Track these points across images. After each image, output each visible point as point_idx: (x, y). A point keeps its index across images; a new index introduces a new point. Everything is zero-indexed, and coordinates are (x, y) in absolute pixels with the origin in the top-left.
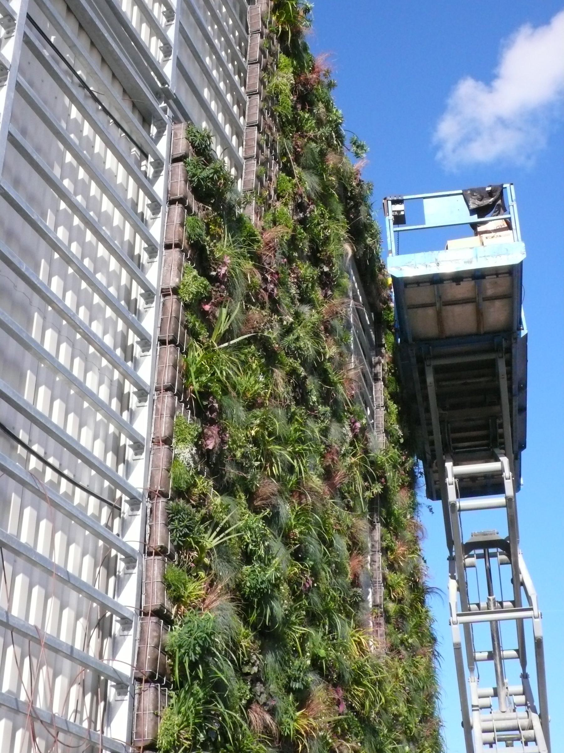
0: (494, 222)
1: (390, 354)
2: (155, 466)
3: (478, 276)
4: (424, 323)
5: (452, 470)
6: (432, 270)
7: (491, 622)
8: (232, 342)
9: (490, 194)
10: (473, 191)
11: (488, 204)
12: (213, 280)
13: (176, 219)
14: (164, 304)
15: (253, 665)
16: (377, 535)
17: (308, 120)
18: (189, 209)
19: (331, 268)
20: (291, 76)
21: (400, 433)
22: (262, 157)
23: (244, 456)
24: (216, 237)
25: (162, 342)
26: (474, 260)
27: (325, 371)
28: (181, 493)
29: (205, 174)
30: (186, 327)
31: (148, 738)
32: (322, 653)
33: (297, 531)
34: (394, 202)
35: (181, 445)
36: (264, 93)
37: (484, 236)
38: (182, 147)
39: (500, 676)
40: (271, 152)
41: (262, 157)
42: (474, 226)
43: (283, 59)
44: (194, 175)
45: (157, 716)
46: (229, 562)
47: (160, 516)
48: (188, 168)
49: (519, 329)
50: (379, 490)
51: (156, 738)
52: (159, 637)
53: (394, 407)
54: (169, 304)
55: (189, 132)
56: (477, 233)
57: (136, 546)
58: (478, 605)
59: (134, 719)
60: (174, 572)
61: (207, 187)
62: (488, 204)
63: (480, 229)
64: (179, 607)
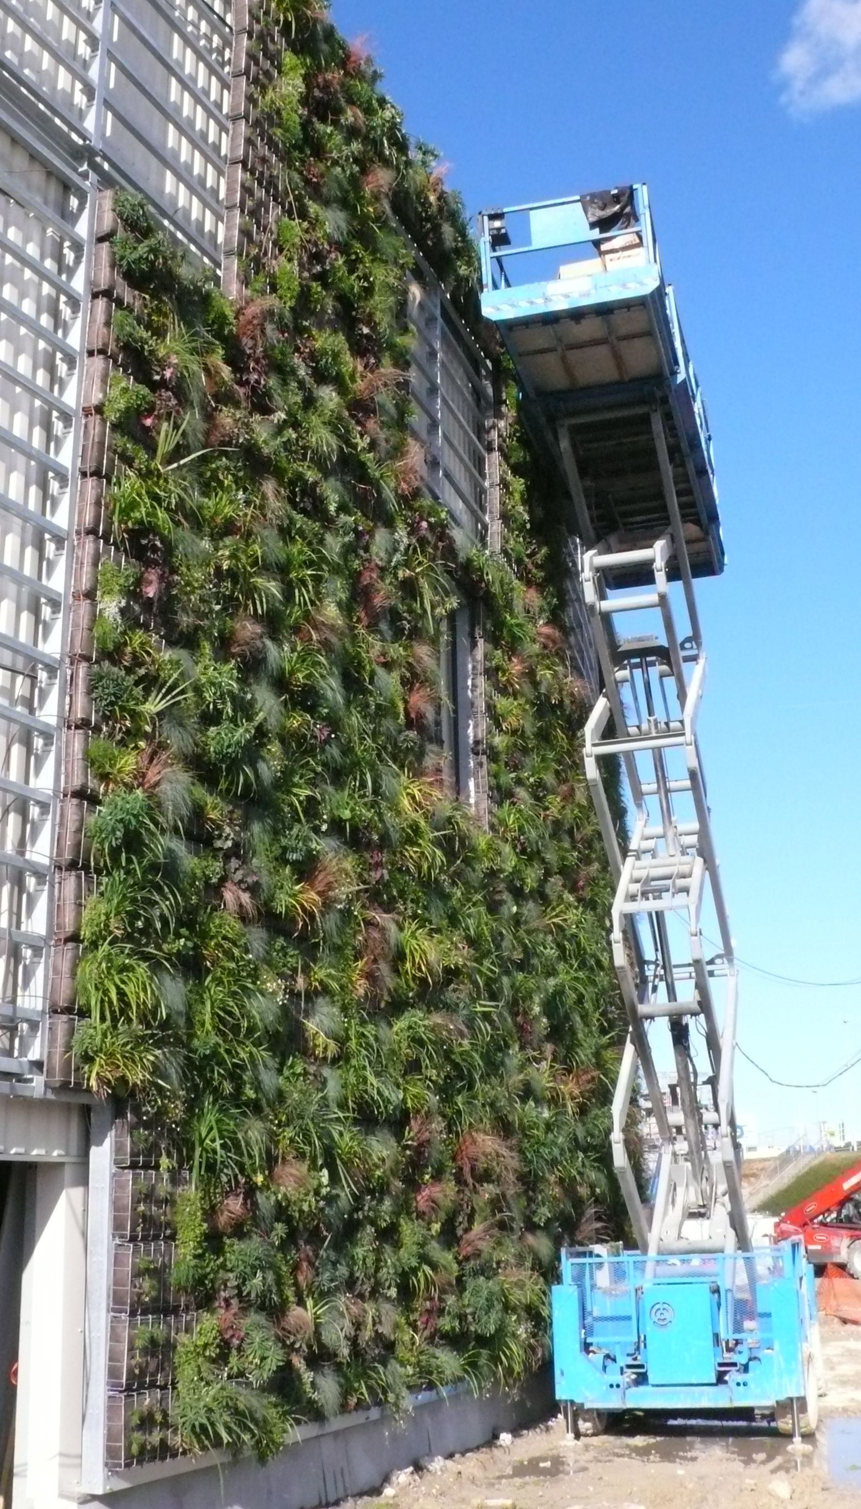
0: (621, 237)
1: (513, 413)
2: (76, 625)
3: (604, 310)
4: (552, 373)
5: (590, 561)
6: (540, 308)
7: (653, 749)
8: (182, 462)
9: (616, 199)
10: (593, 196)
11: (614, 213)
12: (154, 387)
13: (100, 317)
14: (86, 426)
15: (227, 839)
16: (479, 653)
17: (330, 135)
18: (119, 302)
19: (373, 329)
20: (299, 82)
21: (526, 517)
22: (249, 203)
23: (202, 600)
24: (159, 333)
25: (84, 474)
26: (593, 291)
27: (363, 465)
28: (112, 655)
29: (135, 256)
30: (115, 452)
31: (69, 929)
32: (347, 814)
33: (300, 676)
34: (492, 217)
35: (107, 598)
36: (253, 114)
37: (608, 257)
38: (108, 220)
39: (667, 813)
40: (267, 192)
41: (249, 203)
42: (597, 243)
43: (289, 59)
44: (122, 258)
45: (80, 905)
46: (181, 725)
47: (80, 682)
48: (115, 249)
49: (674, 373)
50: (455, 605)
51: (79, 929)
52: (82, 821)
53: (518, 484)
54: (91, 426)
55: (116, 201)
56: (602, 254)
57: (53, 721)
58: (638, 727)
59: (55, 910)
60: (101, 744)
61: (142, 271)
62: (614, 213)
63: (604, 247)
64: (107, 785)
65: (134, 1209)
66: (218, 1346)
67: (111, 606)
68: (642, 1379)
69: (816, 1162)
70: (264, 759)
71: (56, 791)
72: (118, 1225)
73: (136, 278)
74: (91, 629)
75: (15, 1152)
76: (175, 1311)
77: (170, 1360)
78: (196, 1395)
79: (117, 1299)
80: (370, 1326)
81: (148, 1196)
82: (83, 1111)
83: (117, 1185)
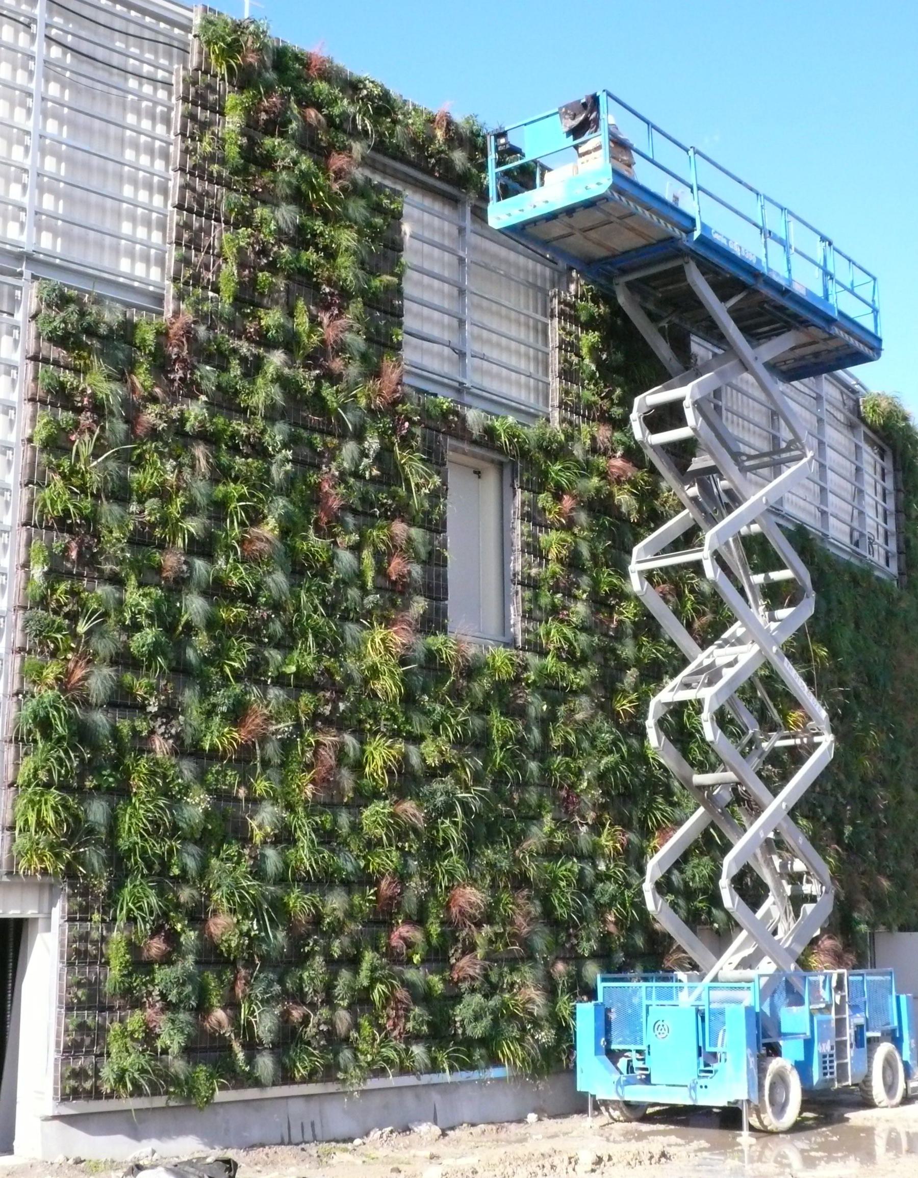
31: (10, 780)
63: (582, 150)
65: (69, 946)
66: (144, 1031)
67: (38, 571)
70: (191, 646)
73: (61, 340)
74: (25, 589)
75: (13, 913)
76: (111, 1009)
77: (104, 1039)
78: (121, 1057)
81: (84, 938)
83: (62, 933)
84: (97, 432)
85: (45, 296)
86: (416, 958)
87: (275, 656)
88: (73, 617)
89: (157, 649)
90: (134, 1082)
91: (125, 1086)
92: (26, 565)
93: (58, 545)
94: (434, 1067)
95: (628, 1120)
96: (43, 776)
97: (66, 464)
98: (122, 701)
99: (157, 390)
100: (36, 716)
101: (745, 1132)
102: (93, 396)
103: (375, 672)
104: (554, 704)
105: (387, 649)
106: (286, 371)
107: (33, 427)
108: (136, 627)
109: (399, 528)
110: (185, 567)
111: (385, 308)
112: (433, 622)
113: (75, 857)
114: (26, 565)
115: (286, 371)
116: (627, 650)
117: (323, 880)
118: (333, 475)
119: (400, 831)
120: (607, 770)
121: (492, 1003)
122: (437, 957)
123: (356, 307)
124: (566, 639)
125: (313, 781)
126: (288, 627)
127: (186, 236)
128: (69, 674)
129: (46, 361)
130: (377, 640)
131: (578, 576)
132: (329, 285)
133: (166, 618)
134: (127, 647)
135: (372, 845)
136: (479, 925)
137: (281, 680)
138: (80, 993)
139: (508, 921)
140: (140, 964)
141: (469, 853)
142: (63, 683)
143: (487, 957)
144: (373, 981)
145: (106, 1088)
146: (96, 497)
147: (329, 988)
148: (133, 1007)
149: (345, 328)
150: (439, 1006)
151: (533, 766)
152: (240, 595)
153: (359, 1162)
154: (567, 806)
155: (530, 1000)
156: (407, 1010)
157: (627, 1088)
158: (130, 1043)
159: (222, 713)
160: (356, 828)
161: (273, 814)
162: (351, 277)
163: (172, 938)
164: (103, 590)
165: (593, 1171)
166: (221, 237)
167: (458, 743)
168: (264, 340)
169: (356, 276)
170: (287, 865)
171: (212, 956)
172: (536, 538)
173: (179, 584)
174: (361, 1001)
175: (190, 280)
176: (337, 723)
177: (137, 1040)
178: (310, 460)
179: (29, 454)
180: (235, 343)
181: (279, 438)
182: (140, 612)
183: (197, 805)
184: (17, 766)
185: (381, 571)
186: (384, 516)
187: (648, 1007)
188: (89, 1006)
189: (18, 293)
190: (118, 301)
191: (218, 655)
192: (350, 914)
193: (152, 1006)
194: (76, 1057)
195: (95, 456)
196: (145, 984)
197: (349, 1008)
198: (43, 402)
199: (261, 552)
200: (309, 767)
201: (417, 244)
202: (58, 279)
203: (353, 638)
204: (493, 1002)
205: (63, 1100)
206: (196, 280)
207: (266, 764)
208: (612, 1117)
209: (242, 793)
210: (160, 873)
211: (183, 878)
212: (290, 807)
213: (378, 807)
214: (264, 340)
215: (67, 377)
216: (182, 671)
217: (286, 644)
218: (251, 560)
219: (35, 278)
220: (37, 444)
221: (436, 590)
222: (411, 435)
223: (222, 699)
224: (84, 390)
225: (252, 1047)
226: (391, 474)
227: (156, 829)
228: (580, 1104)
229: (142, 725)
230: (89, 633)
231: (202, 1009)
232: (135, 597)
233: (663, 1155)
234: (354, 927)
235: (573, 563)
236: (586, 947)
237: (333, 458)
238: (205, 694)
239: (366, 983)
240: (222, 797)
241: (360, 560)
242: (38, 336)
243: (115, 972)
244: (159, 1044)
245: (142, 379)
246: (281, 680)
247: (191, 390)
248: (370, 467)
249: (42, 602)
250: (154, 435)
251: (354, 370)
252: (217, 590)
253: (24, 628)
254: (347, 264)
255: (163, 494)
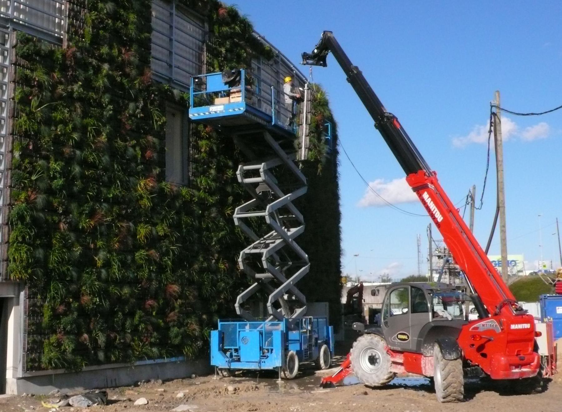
31: (6, 240)
67: (17, 154)
68: (239, 360)
69: (517, 280)
71: (3, 205)
72: (25, 313)
73: (26, 57)
74: (12, 161)
76: (45, 334)
78: (48, 354)
79: (25, 331)
80: (89, 18)
82: (19, 285)
83: (25, 303)
84: (41, 96)
85: (20, 37)
86: (154, 313)
87: (104, 190)
88: (31, 174)
89: (63, 187)
90: (55, 363)
91: (51, 365)
92: (12, 152)
93: (25, 142)
94: (161, 356)
95: (229, 376)
96: (20, 239)
97: (28, 109)
98: (49, 208)
99: (62, 79)
100: (18, 213)
101: (280, 379)
102: (38, 81)
103: (142, 197)
104: (203, 212)
105: (146, 188)
106: (110, 72)
107: (15, 93)
108: (55, 178)
109: (150, 138)
110: (72, 153)
111: (145, 46)
112: (161, 177)
113: (32, 272)
114: (12, 152)
115: (110, 72)
116: (229, 189)
117: (121, 283)
118: (127, 116)
119: (149, 260)
120: (222, 237)
121: (181, 331)
122: (162, 313)
123: (135, 47)
124: (208, 184)
125: (118, 242)
126: (110, 178)
127: (72, 14)
128: (29, 197)
129: (19, 65)
130: (142, 184)
131: (212, 158)
132: (125, 37)
133: (65, 173)
134: (51, 186)
135: (140, 267)
136: (176, 300)
137: (107, 200)
138: (33, 328)
139: (187, 298)
140: (56, 316)
141: (173, 271)
142: (27, 200)
143: (179, 312)
144: (140, 322)
145: (43, 365)
146: (39, 123)
147: (124, 324)
148: (52, 333)
149: (131, 56)
150: (164, 331)
151: (196, 235)
152: (93, 166)
153: (136, 394)
154: (207, 251)
155: (194, 330)
156: (151, 334)
157: (232, 363)
158: (52, 348)
159: (86, 214)
160: (133, 260)
161: (104, 255)
162: (133, 34)
163: (68, 305)
164: (41, 162)
165: (235, 393)
166: (84, 13)
167: (170, 226)
168: (101, 59)
169: (135, 33)
170: (109, 275)
171: (83, 312)
172: (198, 143)
173: (69, 161)
174: (135, 330)
175: (74, 32)
176: (127, 218)
177: (54, 346)
178: (118, 111)
179: (13, 105)
180: (90, 60)
181: (107, 100)
182: (56, 172)
183: (78, 250)
184: (9, 235)
185: (143, 156)
186: (144, 133)
187: (239, 332)
188: (36, 333)
189: (7, 36)
190: (47, 41)
191: (84, 190)
192: (131, 296)
193: (60, 333)
194: (32, 354)
195: (39, 106)
196: (58, 324)
197: (131, 333)
198: (18, 83)
199: (101, 147)
200: (117, 236)
201: (158, 21)
202: (25, 31)
203: (133, 183)
204: (182, 330)
205: (27, 370)
206: (76, 33)
207: (101, 234)
208: (223, 375)
209: (92, 246)
210: (62, 278)
211: (71, 281)
212: (110, 252)
213: (143, 252)
214: (101, 59)
215: (28, 72)
216: (72, 197)
217: (109, 185)
218: (97, 150)
219: (14, 30)
220: (17, 101)
221: (162, 164)
222: (154, 100)
223: (86, 208)
224: (35, 79)
225: (96, 347)
226: (148, 116)
227: (62, 262)
228: (211, 370)
229: (56, 218)
230: (36, 180)
231: (79, 334)
232: (56, 166)
233: (256, 387)
234: (133, 300)
235: (210, 153)
236: (215, 307)
237: (126, 109)
238: (80, 205)
239: (137, 323)
240: (86, 247)
241: (135, 151)
242: (17, 55)
243: (46, 319)
244: (63, 347)
245: (56, 75)
246: (107, 200)
247: (74, 80)
248: (139, 113)
249: (19, 167)
250: (61, 97)
251: (134, 73)
252: (84, 163)
253: (11, 178)
254: (132, 28)
255: (64, 122)
